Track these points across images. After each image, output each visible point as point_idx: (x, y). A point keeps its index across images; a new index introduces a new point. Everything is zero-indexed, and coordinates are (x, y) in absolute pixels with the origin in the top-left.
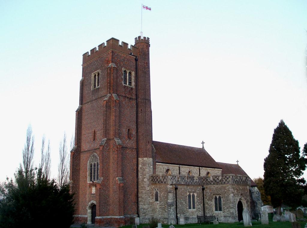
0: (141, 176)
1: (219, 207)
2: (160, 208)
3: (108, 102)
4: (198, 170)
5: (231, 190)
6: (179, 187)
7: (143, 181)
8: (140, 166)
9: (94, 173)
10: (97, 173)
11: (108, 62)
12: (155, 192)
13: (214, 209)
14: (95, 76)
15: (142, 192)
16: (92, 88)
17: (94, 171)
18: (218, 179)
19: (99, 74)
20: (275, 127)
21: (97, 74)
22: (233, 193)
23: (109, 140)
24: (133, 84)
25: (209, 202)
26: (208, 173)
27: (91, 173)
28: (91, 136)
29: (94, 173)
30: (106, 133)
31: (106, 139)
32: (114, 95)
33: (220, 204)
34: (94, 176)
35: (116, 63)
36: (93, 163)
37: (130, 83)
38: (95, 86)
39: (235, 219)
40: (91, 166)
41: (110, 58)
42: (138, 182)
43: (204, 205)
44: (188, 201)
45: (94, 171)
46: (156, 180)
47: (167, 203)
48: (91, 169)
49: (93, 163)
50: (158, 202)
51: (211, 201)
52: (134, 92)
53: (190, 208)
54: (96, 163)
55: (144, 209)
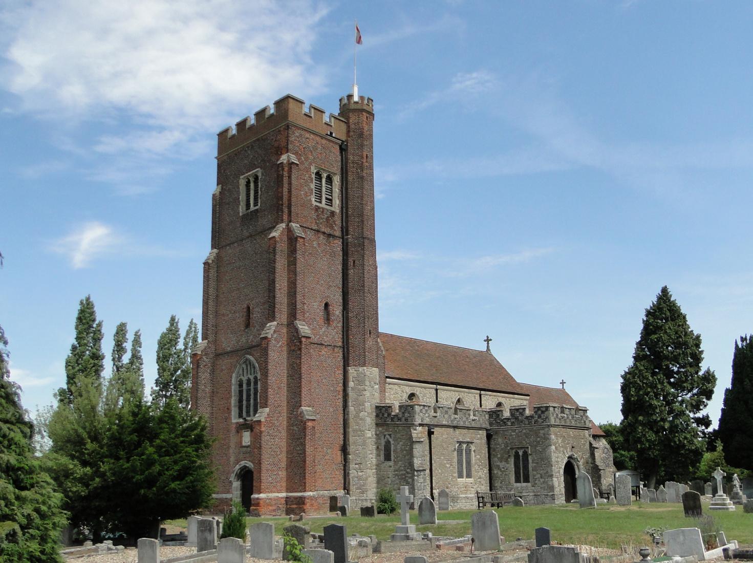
2: (396, 475)
4: (478, 397)
9: (248, 400)
10: (256, 399)
13: (513, 478)
14: (248, 183)
21: (252, 180)
24: (337, 202)
25: (502, 465)
28: (240, 319)
29: (248, 400)
33: (526, 467)
34: (248, 407)
36: (244, 379)
37: (330, 201)
40: (241, 385)
44: (455, 460)
46: (386, 415)
48: (241, 392)
49: (244, 379)
50: (391, 463)
54: (252, 377)
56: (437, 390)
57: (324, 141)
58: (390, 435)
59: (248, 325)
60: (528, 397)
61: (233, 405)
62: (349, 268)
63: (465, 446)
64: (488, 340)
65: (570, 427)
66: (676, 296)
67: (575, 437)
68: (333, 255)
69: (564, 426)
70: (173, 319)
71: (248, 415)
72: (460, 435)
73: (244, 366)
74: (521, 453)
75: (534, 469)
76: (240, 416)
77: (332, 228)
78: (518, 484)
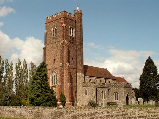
0: (78, 82)
1: (117, 99)
2: (88, 98)
3: (63, 44)
4: (105, 80)
5: (123, 90)
6: (98, 88)
7: (79, 85)
8: (78, 77)
9: (54, 81)
10: (56, 81)
11: (62, 23)
12: (85, 91)
13: (114, 99)
14: (54, 30)
15: (79, 91)
16: (52, 36)
17: (54, 80)
18: (117, 84)
19: (56, 29)
20: (146, 59)
21: (55, 29)
22: (124, 91)
23: (63, 64)
24: (74, 35)
25: (112, 96)
26: (109, 82)
27: (52, 81)
28: (52, 62)
29: (54, 81)
30: (62, 61)
31: (62, 63)
32: (66, 41)
33: (117, 97)
34: (54, 82)
35: (66, 24)
36: (53, 76)
37: (73, 34)
38: (54, 35)
39: (125, 104)
40: (52, 77)
41: (63, 22)
42: (77, 85)
43: (109, 97)
44: (101, 95)
45: (54, 80)
46: (86, 85)
47: (92, 96)
48: (52, 79)
49: (53, 76)
50: (87, 96)
51: (26, 99)
52: (75, 40)
53: (103, 99)
54: (55, 75)
55: (80, 99)
56: (96, 78)
57: (72, 21)
58: (87, 89)
59: (54, 63)
60: (116, 80)
61: (50, 81)
62: (59, 87)
63: (103, 92)
64: (106, 66)
65: (128, 88)
66: (151, 58)
67: (129, 90)
68: (74, 47)
69: (126, 88)
70: (19, 60)
71: (54, 84)
72: (103, 89)
73: (53, 73)
74: (116, 93)
75: (120, 97)
76: (52, 84)
77: (73, 41)
78: (116, 101)
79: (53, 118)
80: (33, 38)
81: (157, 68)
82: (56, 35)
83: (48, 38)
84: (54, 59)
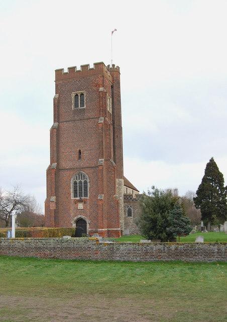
19: (82, 94)
36: (78, 181)
46: (129, 199)
49: (78, 181)
50: (132, 217)
59: (80, 158)
76: (75, 196)
79: (98, 318)
80: (181, 194)
81: (224, 177)
82: (82, 105)
83: (63, 109)
84: (80, 152)
